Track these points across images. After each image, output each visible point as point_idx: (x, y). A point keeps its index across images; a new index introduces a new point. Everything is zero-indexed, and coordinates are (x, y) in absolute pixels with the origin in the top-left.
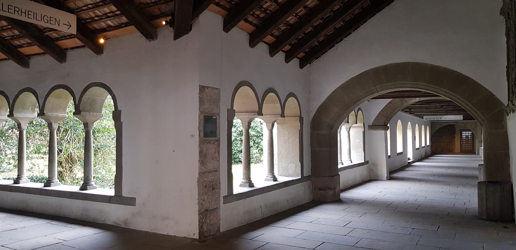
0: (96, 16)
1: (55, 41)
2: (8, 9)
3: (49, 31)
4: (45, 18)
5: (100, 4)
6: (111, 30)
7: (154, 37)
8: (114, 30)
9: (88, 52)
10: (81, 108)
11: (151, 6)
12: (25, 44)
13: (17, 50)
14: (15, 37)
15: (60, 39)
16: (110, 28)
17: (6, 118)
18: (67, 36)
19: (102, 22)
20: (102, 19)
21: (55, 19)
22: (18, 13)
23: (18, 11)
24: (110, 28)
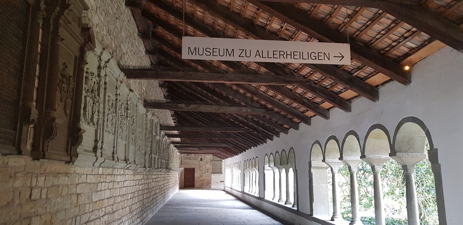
0: (394, 41)
1: (364, 80)
2: (274, 54)
3: (356, 72)
4: (313, 54)
5: (392, 26)
6: (414, 53)
7: (345, 30)
8: (417, 51)
9: (395, 85)
10: (396, 148)
11: (453, 6)
12: (343, 89)
13: (339, 96)
14: (333, 84)
15: (368, 77)
16: (413, 51)
17: (338, 160)
18: (373, 72)
19: (400, 46)
20: (399, 43)
21: (324, 53)
22: (283, 56)
23: (283, 55)
24: (413, 51)
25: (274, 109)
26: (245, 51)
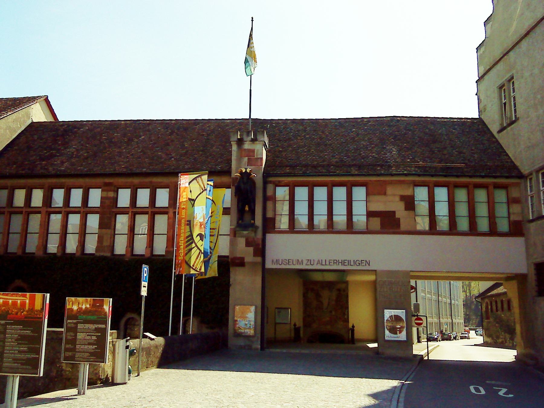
4: (358, 262)
21: (366, 261)
25: (114, 194)
26: (310, 260)
